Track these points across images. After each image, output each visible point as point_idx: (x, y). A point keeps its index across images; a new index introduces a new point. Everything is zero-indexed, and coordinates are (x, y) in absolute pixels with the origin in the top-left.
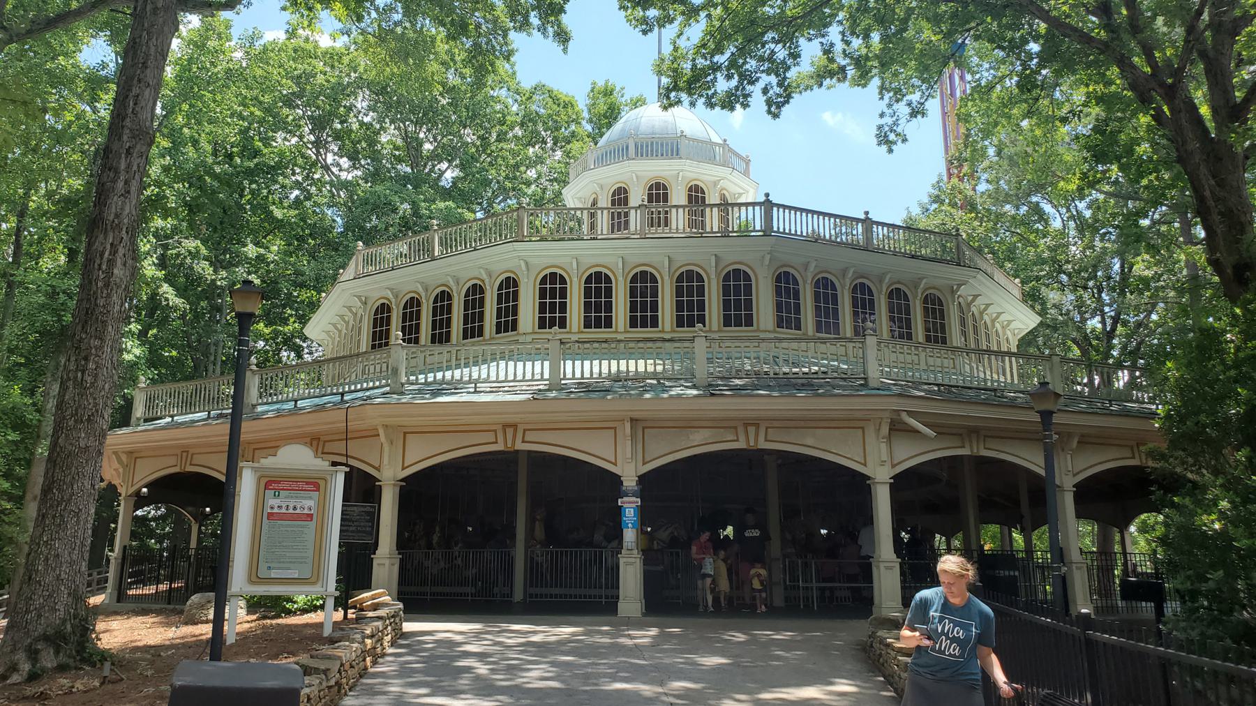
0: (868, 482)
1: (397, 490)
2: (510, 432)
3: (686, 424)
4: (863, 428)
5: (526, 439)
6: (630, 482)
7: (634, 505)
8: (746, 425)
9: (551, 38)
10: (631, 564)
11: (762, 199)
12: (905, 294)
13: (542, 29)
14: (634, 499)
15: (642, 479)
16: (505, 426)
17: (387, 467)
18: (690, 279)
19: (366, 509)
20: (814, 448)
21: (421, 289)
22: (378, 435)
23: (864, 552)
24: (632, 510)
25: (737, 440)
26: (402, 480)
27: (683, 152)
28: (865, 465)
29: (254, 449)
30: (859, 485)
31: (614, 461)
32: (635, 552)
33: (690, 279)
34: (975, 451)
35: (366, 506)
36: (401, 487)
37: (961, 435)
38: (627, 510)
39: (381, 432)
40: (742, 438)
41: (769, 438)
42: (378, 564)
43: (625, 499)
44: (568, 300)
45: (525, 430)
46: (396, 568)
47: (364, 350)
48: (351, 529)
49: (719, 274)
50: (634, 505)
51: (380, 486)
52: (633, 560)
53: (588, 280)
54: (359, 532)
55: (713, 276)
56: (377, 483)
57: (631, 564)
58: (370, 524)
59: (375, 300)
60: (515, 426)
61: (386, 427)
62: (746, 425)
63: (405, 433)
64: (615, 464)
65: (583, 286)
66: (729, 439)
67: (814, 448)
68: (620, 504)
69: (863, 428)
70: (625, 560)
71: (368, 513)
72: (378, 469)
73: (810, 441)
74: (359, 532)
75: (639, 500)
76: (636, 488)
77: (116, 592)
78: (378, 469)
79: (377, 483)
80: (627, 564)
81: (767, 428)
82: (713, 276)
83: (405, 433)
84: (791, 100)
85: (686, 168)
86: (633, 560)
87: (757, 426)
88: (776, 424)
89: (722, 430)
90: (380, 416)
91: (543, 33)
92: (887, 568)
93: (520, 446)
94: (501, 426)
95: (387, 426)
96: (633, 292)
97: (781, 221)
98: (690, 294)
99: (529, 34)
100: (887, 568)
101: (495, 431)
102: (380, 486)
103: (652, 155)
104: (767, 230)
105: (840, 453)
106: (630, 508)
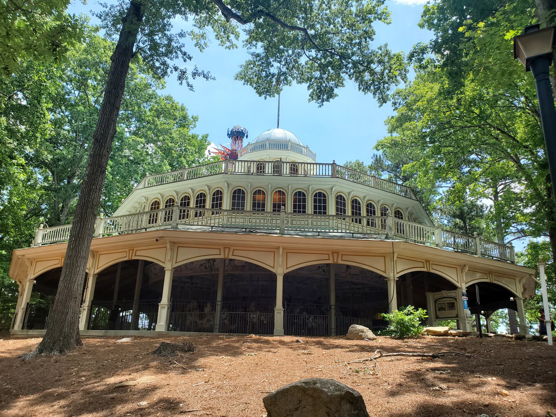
4: (515, 279)
8: (489, 273)
11: (332, 163)
12: (344, 198)
14: (465, 297)
18: (320, 196)
21: (160, 197)
23: (434, 323)
27: (289, 148)
29: (234, 250)
30: (383, 281)
33: (320, 196)
34: (336, 261)
37: (486, 274)
44: (313, 204)
47: (147, 211)
49: (252, 192)
50: (466, 300)
51: (387, 281)
53: (315, 196)
55: (249, 192)
59: (152, 199)
64: (273, 268)
65: (313, 198)
69: (515, 279)
82: (249, 192)
85: (290, 155)
88: (496, 274)
93: (340, 262)
94: (330, 253)
96: (315, 201)
98: (320, 202)
101: (328, 254)
103: (283, 149)
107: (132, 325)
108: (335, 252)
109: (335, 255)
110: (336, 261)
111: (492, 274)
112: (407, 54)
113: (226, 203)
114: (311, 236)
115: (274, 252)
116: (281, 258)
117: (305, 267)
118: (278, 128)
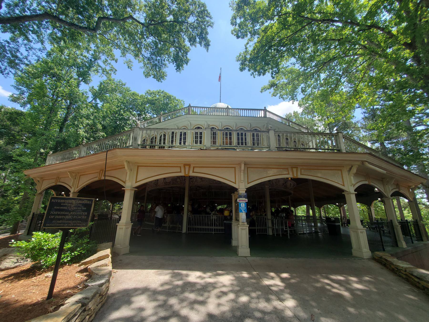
0: (343, 193)
1: (133, 192)
2: (187, 167)
3: (266, 166)
4: (341, 170)
5: (195, 171)
6: (242, 191)
7: (244, 202)
8: (292, 168)
9: (203, 46)
10: (244, 229)
13: (200, 43)
14: (244, 199)
15: (248, 190)
16: (185, 165)
17: (128, 181)
19: (83, 202)
20: (321, 178)
22: (125, 168)
24: (244, 204)
25: (289, 174)
26: (136, 188)
28: (344, 185)
31: (234, 182)
32: (246, 223)
35: (83, 200)
36: (135, 191)
37: (287, 169)
38: (241, 204)
39: (125, 164)
40: (291, 173)
41: (302, 173)
42: (120, 228)
43: (241, 199)
45: (194, 167)
46: (129, 230)
48: (67, 217)
50: (244, 202)
51: (124, 190)
52: (245, 227)
54: (75, 219)
56: (122, 189)
57: (244, 229)
58: (86, 213)
60: (189, 165)
61: (128, 162)
62: (292, 168)
63: (138, 166)
64: (235, 183)
66: (285, 173)
67: (321, 178)
68: (238, 201)
69: (341, 170)
70: (241, 227)
71: (85, 205)
72: (124, 182)
73: (319, 175)
74: (75, 219)
75: (247, 199)
76: (245, 194)
77: (27, 231)
78: (124, 182)
79: (122, 189)
80: (242, 229)
81: (301, 169)
83: (138, 166)
84: (261, 90)
86: (245, 227)
87: (297, 168)
88: (305, 167)
89: (282, 170)
90: (124, 155)
91: (200, 44)
92: (361, 232)
95: (129, 162)
97: (268, 115)
99: (195, 46)
100: (361, 232)
101: (180, 167)
102: (124, 190)
104: (265, 116)
105: (333, 180)
106: (243, 203)
107: (236, 275)
108: (187, 165)
109: (187, 167)
110: (187, 173)
111: (297, 168)
112: (271, 78)
113: (190, 139)
114: (322, 152)
115: (235, 168)
116: (242, 174)
117: (149, 182)
118: (220, 102)
